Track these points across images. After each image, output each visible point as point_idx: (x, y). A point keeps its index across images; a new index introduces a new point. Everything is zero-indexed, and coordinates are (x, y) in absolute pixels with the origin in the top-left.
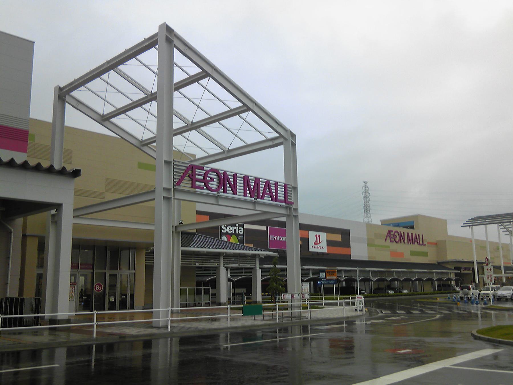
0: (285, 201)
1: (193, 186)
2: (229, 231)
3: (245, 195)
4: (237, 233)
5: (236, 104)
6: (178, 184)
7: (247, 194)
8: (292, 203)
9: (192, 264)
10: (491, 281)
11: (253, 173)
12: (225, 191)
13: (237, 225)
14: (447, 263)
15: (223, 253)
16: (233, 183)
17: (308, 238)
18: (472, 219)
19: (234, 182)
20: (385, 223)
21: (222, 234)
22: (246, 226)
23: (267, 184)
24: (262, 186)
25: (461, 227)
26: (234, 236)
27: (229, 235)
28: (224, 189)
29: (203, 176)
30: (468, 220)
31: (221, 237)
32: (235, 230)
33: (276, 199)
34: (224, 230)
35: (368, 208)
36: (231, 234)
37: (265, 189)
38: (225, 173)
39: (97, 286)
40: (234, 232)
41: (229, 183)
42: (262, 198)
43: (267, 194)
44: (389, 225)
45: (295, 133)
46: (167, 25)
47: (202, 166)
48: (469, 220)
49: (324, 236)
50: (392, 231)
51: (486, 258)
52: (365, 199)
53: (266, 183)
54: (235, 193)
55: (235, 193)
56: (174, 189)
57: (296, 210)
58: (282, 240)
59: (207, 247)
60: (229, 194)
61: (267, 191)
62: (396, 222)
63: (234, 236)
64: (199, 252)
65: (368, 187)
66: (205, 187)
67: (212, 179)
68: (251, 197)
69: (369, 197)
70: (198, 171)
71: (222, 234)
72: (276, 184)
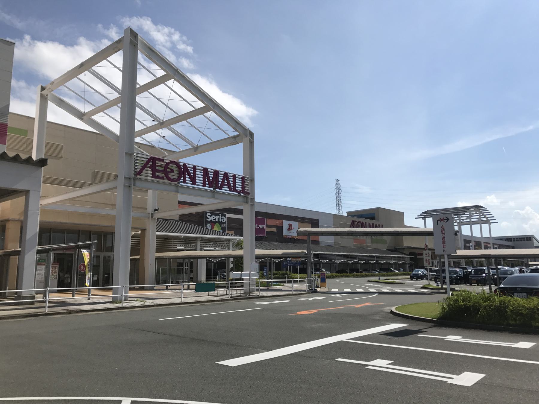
0: (243, 191)
1: (154, 176)
2: (213, 219)
3: (204, 185)
4: (220, 221)
5: (200, 105)
6: (139, 173)
7: (206, 184)
8: (249, 193)
9: (171, 247)
10: (429, 264)
11: (212, 166)
12: (184, 182)
13: (220, 215)
14: (404, 249)
15: (200, 238)
16: (192, 174)
17: (282, 227)
18: (425, 212)
19: (193, 173)
20: (350, 214)
21: (208, 222)
22: (228, 215)
23: (226, 175)
24: (221, 178)
25: (416, 218)
26: (217, 224)
27: (213, 223)
28: (183, 180)
29: (164, 167)
30: (422, 213)
31: (206, 225)
32: (219, 219)
33: (234, 190)
34: (208, 218)
35: (340, 202)
36: (215, 222)
37: (223, 180)
38: (185, 165)
39: (81, 266)
40: (217, 220)
41: (189, 174)
42: (221, 188)
43: (226, 185)
44: (353, 216)
45: (253, 132)
46: (131, 29)
47: (163, 158)
48: (423, 213)
49: (295, 224)
50: (356, 221)
51: (426, 244)
52: (338, 195)
53: (224, 175)
54: (194, 183)
55: (194, 183)
56: (135, 179)
57: (253, 199)
58: (260, 227)
59: (174, 232)
60: (189, 183)
61: (226, 182)
62: (360, 214)
63: (217, 224)
64: (177, 236)
65: (340, 185)
66: (165, 178)
67: (172, 171)
68: (210, 187)
69: (341, 193)
70: (158, 163)
71: (208, 222)
72: (234, 176)
